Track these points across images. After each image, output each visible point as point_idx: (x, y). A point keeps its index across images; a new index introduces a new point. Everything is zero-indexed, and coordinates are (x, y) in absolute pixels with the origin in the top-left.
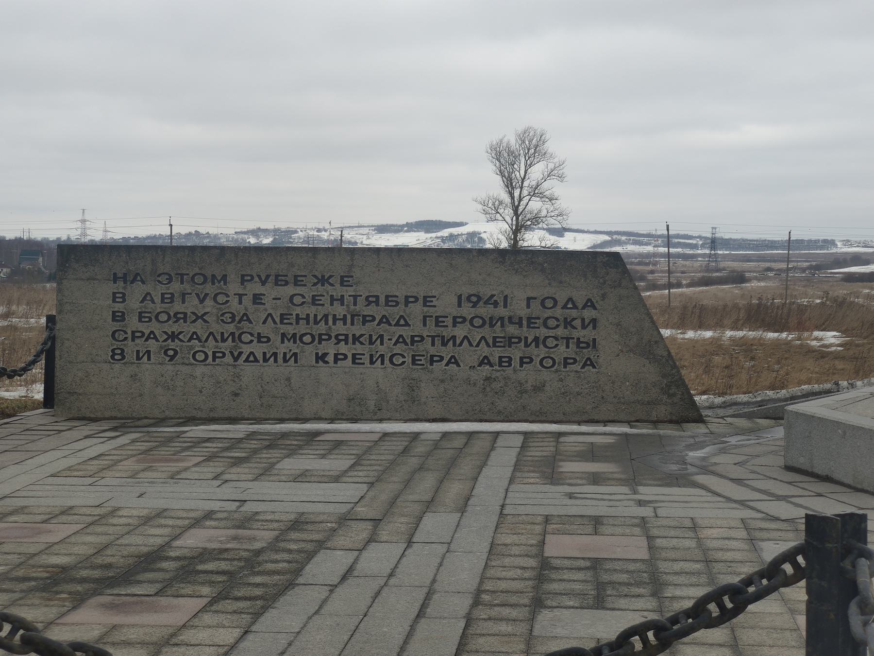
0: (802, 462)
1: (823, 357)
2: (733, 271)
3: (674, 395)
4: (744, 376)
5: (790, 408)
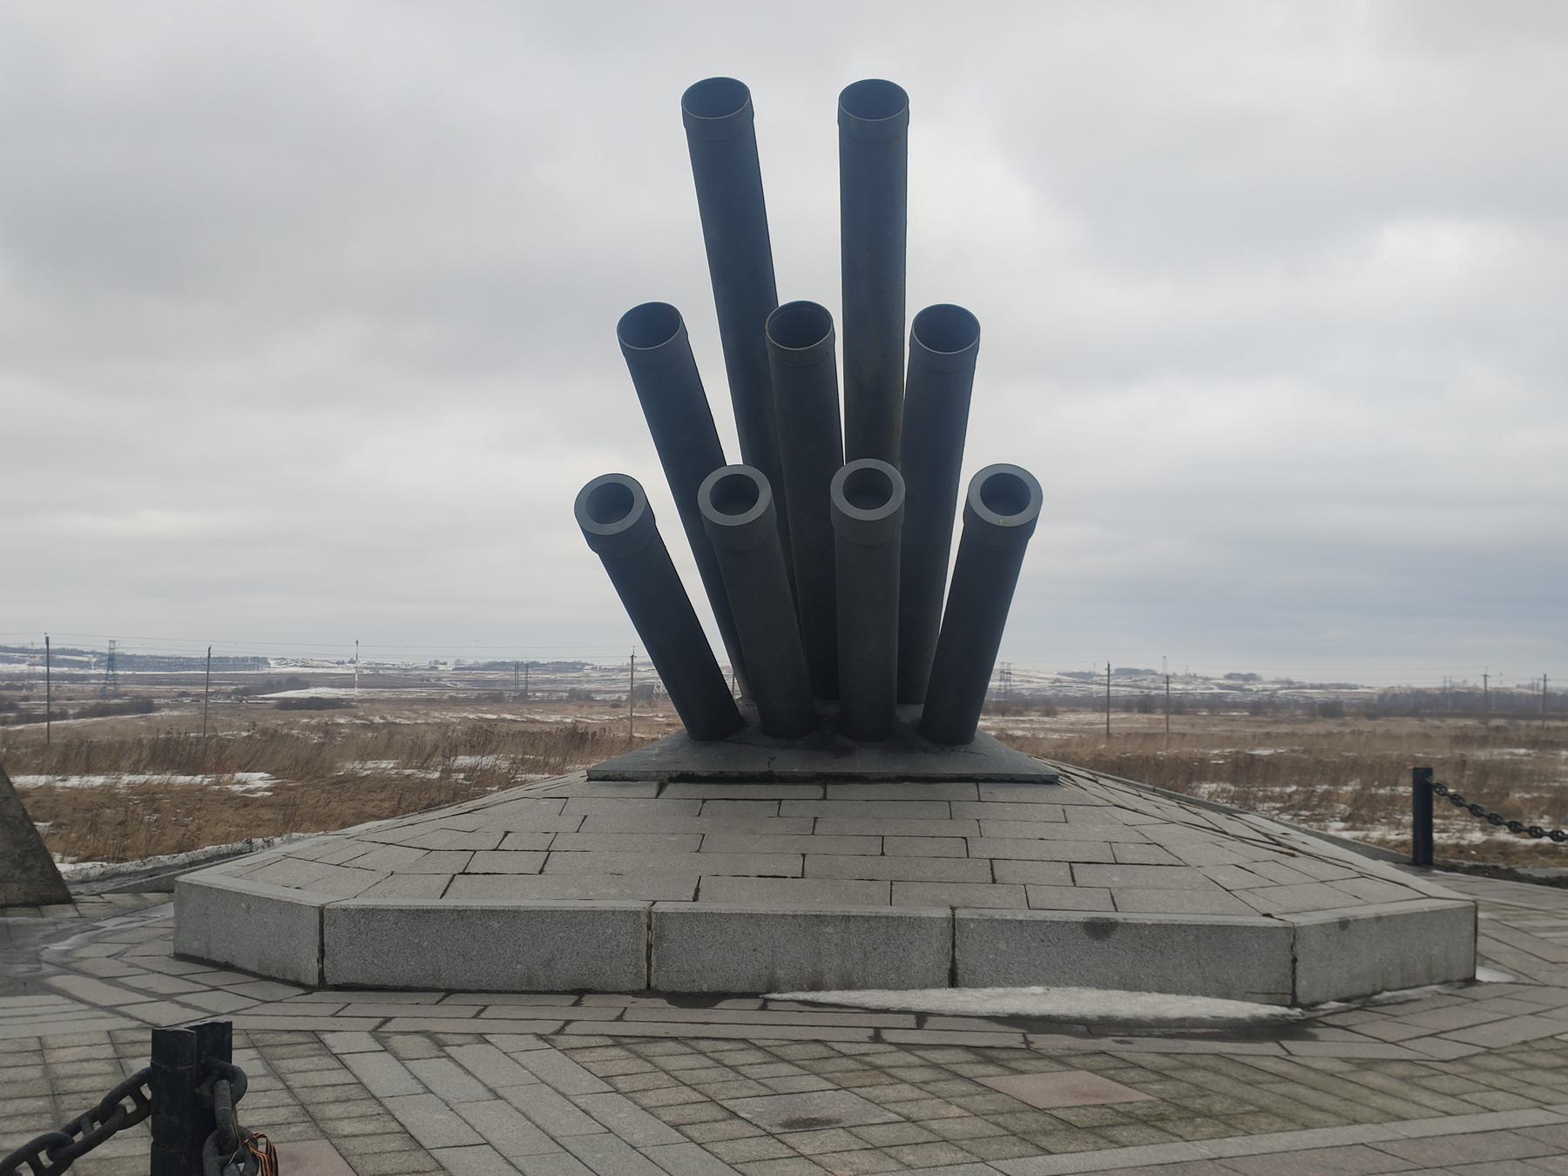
0: (196, 947)
1: (246, 806)
2: (137, 697)
3: (31, 868)
4: (143, 835)
5: (182, 878)
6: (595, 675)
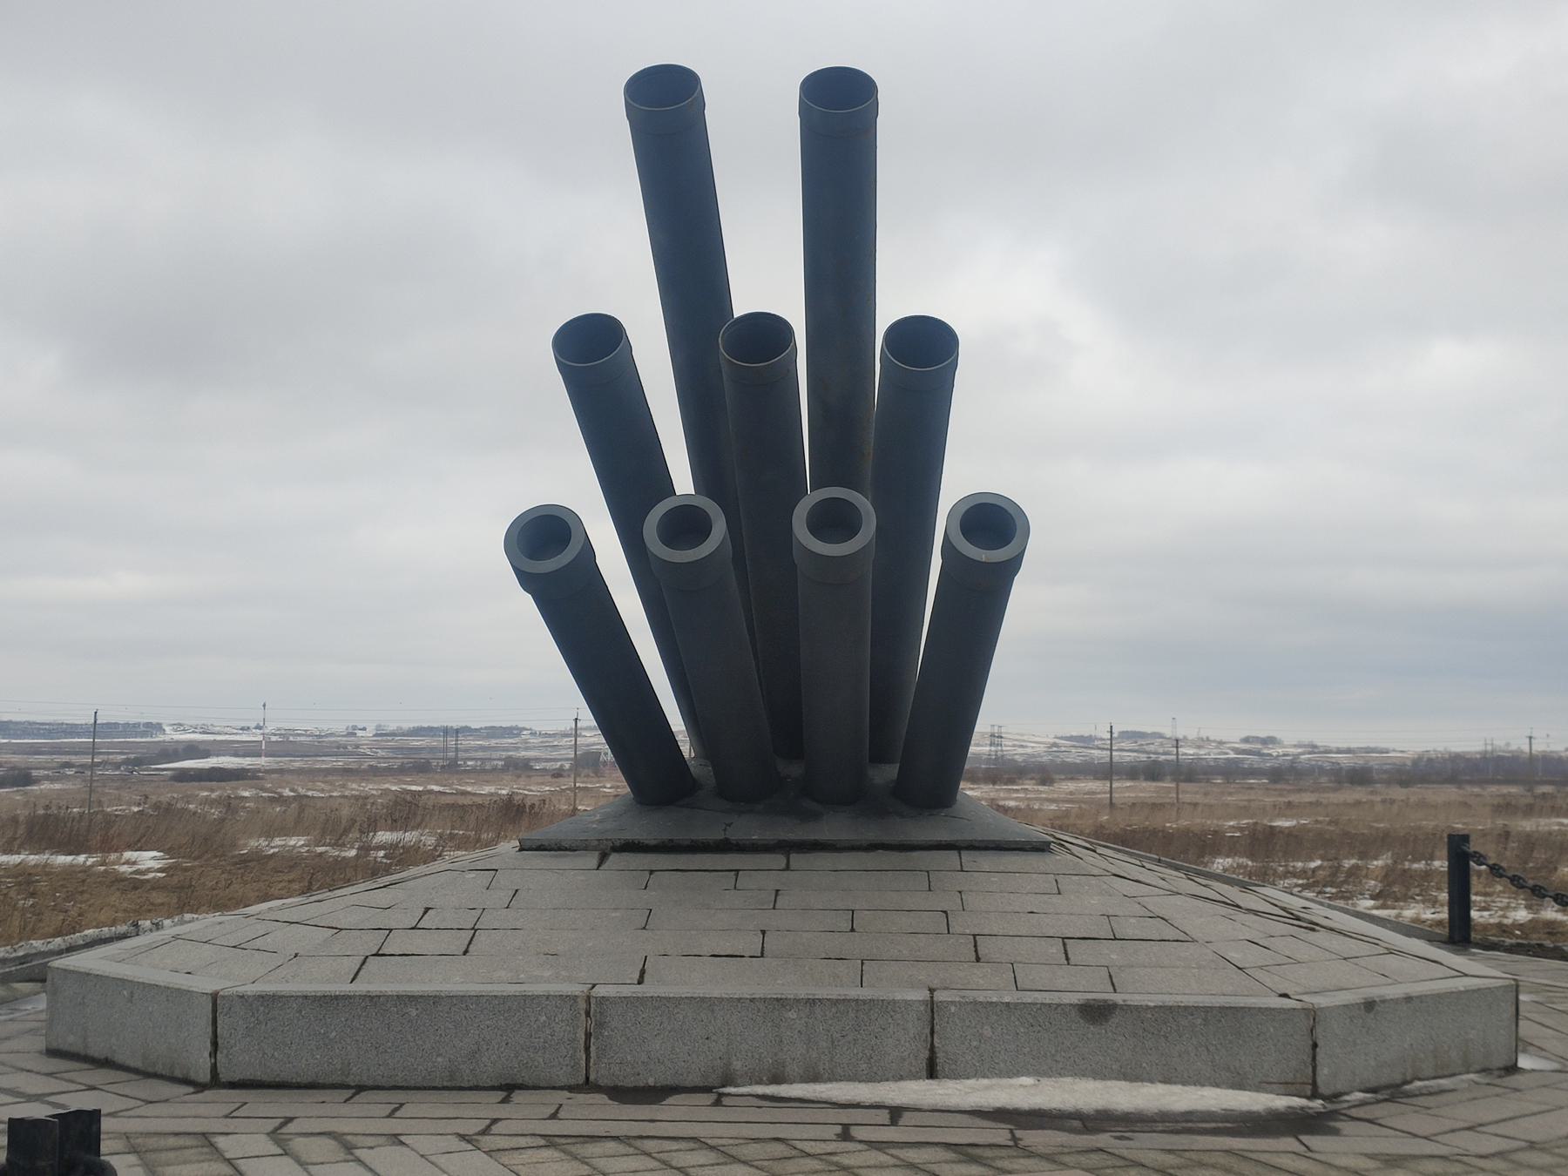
0: (71, 1042)
1: (135, 888)
2: (13, 768)
6: (534, 741)
